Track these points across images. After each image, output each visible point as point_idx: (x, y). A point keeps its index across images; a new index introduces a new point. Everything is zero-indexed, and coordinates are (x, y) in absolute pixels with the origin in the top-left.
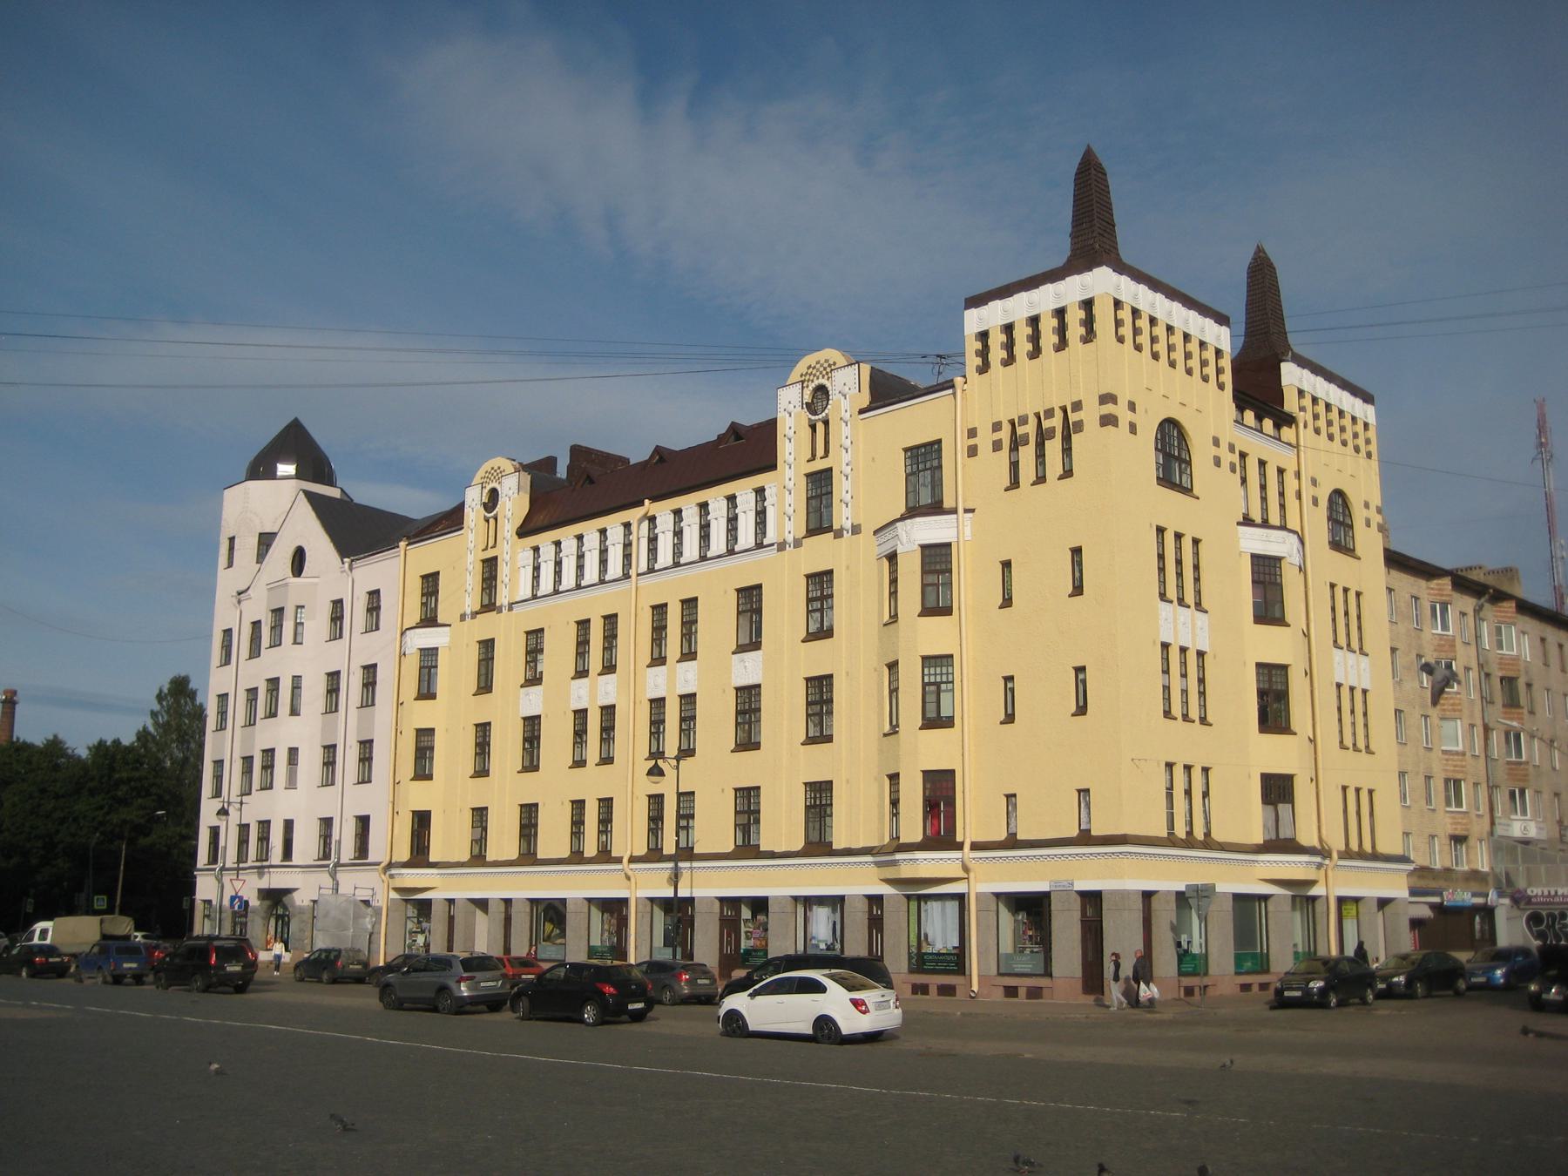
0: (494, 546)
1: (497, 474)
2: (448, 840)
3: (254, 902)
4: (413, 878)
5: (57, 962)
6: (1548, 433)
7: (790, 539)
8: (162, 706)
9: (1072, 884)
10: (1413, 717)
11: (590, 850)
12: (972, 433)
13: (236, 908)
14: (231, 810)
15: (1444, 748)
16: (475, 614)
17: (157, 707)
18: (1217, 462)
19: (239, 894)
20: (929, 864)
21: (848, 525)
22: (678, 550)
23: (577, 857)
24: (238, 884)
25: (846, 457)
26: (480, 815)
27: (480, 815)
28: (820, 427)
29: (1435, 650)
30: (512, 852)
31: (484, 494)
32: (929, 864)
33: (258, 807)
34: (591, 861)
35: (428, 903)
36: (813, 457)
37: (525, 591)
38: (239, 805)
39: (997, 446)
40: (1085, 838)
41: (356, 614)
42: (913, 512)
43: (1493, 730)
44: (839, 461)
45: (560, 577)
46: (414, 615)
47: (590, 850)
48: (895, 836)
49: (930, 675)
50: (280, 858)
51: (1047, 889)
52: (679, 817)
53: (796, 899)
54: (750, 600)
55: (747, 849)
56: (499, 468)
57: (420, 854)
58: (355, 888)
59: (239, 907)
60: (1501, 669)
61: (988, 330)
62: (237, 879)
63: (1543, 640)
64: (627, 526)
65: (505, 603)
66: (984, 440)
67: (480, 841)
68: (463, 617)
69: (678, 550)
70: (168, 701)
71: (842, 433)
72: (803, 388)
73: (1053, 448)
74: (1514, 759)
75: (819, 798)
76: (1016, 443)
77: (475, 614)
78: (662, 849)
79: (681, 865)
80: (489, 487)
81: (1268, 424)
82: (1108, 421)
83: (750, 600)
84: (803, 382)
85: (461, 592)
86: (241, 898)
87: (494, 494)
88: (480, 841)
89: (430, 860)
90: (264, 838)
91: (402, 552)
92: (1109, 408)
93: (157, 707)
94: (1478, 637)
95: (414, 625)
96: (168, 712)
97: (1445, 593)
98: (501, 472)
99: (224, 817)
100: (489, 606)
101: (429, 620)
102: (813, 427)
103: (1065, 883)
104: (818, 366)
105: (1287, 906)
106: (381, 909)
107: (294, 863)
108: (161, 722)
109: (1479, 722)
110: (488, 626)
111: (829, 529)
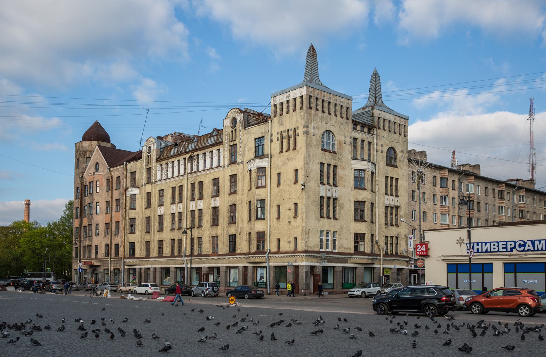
0: (235, 140)
2: (139, 251)
6: (534, 110)
7: (226, 165)
10: (152, 240)
14: (188, 231)
20: (259, 258)
22: (212, 165)
23: (173, 256)
28: (234, 132)
32: (259, 258)
35: (134, 269)
42: (257, 157)
43: (462, 217)
45: (206, 165)
52: (199, 245)
53: (227, 267)
54: (216, 182)
55: (215, 253)
57: (132, 255)
63: (486, 188)
69: (212, 165)
77: (145, 185)
79: (192, 258)
80: (149, 146)
83: (216, 182)
85: (142, 177)
97: (446, 174)
99: (185, 234)
105: (362, 270)
109: (457, 215)
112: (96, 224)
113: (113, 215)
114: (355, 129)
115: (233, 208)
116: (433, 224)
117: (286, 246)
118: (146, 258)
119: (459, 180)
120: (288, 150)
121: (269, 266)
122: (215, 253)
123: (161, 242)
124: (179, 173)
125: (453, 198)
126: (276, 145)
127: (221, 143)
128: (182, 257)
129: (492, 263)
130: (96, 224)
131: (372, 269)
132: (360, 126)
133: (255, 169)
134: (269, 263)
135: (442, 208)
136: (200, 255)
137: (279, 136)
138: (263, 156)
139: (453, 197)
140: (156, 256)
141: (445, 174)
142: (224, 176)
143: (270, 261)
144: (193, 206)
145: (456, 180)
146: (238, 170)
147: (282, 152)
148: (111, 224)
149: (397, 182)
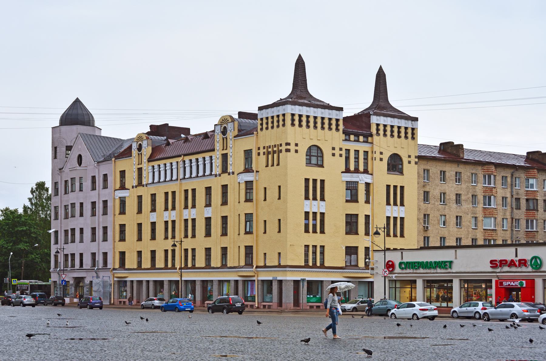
2: (131, 262)
3: (72, 282)
4: (121, 274)
8: (34, 196)
12: (259, 149)
13: (64, 284)
15: (484, 228)
17: (31, 196)
18: (334, 155)
19: (65, 279)
24: (64, 276)
25: (231, 151)
26: (140, 253)
27: (140, 253)
29: (484, 192)
33: (70, 248)
35: (126, 281)
36: (223, 150)
37: (150, 181)
39: (264, 153)
40: (279, 266)
41: (99, 182)
44: (229, 152)
46: (118, 186)
50: (79, 266)
51: (272, 279)
54: (208, 190)
58: (103, 277)
59: (65, 284)
60: (526, 196)
62: (64, 274)
64: (177, 162)
66: (262, 151)
67: (140, 263)
68: (133, 187)
70: (36, 193)
71: (230, 143)
72: (221, 126)
73: (275, 155)
76: (269, 153)
77: (136, 187)
80: (139, 143)
81: (361, 138)
82: (288, 150)
83: (208, 190)
84: (221, 124)
85: (131, 179)
86: (65, 281)
87: (140, 145)
88: (140, 263)
90: (73, 260)
91: (113, 162)
92: (288, 147)
93: (31, 196)
94: (427, 204)
96: (36, 198)
100: (140, 184)
101: (123, 187)
102: (223, 139)
106: (111, 284)
107: (84, 268)
108: (34, 203)
109: (509, 217)
110: (141, 191)
112: (80, 178)
115: (225, 219)
116: (471, 229)
119: (512, 175)
120: (273, 165)
121: (258, 280)
122: (208, 266)
125: (503, 198)
126: (263, 158)
127: (213, 150)
128: (176, 269)
129: (534, 279)
130: (80, 178)
131: (370, 283)
133: (244, 182)
134: (258, 276)
135: (485, 210)
136: (194, 267)
137: (265, 150)
139: (503, 196)
141: (489, 170)
142: (216, 185)
143: (259, 276)
145: (509, 176)
147: (267, 166)
149: (307, 226)
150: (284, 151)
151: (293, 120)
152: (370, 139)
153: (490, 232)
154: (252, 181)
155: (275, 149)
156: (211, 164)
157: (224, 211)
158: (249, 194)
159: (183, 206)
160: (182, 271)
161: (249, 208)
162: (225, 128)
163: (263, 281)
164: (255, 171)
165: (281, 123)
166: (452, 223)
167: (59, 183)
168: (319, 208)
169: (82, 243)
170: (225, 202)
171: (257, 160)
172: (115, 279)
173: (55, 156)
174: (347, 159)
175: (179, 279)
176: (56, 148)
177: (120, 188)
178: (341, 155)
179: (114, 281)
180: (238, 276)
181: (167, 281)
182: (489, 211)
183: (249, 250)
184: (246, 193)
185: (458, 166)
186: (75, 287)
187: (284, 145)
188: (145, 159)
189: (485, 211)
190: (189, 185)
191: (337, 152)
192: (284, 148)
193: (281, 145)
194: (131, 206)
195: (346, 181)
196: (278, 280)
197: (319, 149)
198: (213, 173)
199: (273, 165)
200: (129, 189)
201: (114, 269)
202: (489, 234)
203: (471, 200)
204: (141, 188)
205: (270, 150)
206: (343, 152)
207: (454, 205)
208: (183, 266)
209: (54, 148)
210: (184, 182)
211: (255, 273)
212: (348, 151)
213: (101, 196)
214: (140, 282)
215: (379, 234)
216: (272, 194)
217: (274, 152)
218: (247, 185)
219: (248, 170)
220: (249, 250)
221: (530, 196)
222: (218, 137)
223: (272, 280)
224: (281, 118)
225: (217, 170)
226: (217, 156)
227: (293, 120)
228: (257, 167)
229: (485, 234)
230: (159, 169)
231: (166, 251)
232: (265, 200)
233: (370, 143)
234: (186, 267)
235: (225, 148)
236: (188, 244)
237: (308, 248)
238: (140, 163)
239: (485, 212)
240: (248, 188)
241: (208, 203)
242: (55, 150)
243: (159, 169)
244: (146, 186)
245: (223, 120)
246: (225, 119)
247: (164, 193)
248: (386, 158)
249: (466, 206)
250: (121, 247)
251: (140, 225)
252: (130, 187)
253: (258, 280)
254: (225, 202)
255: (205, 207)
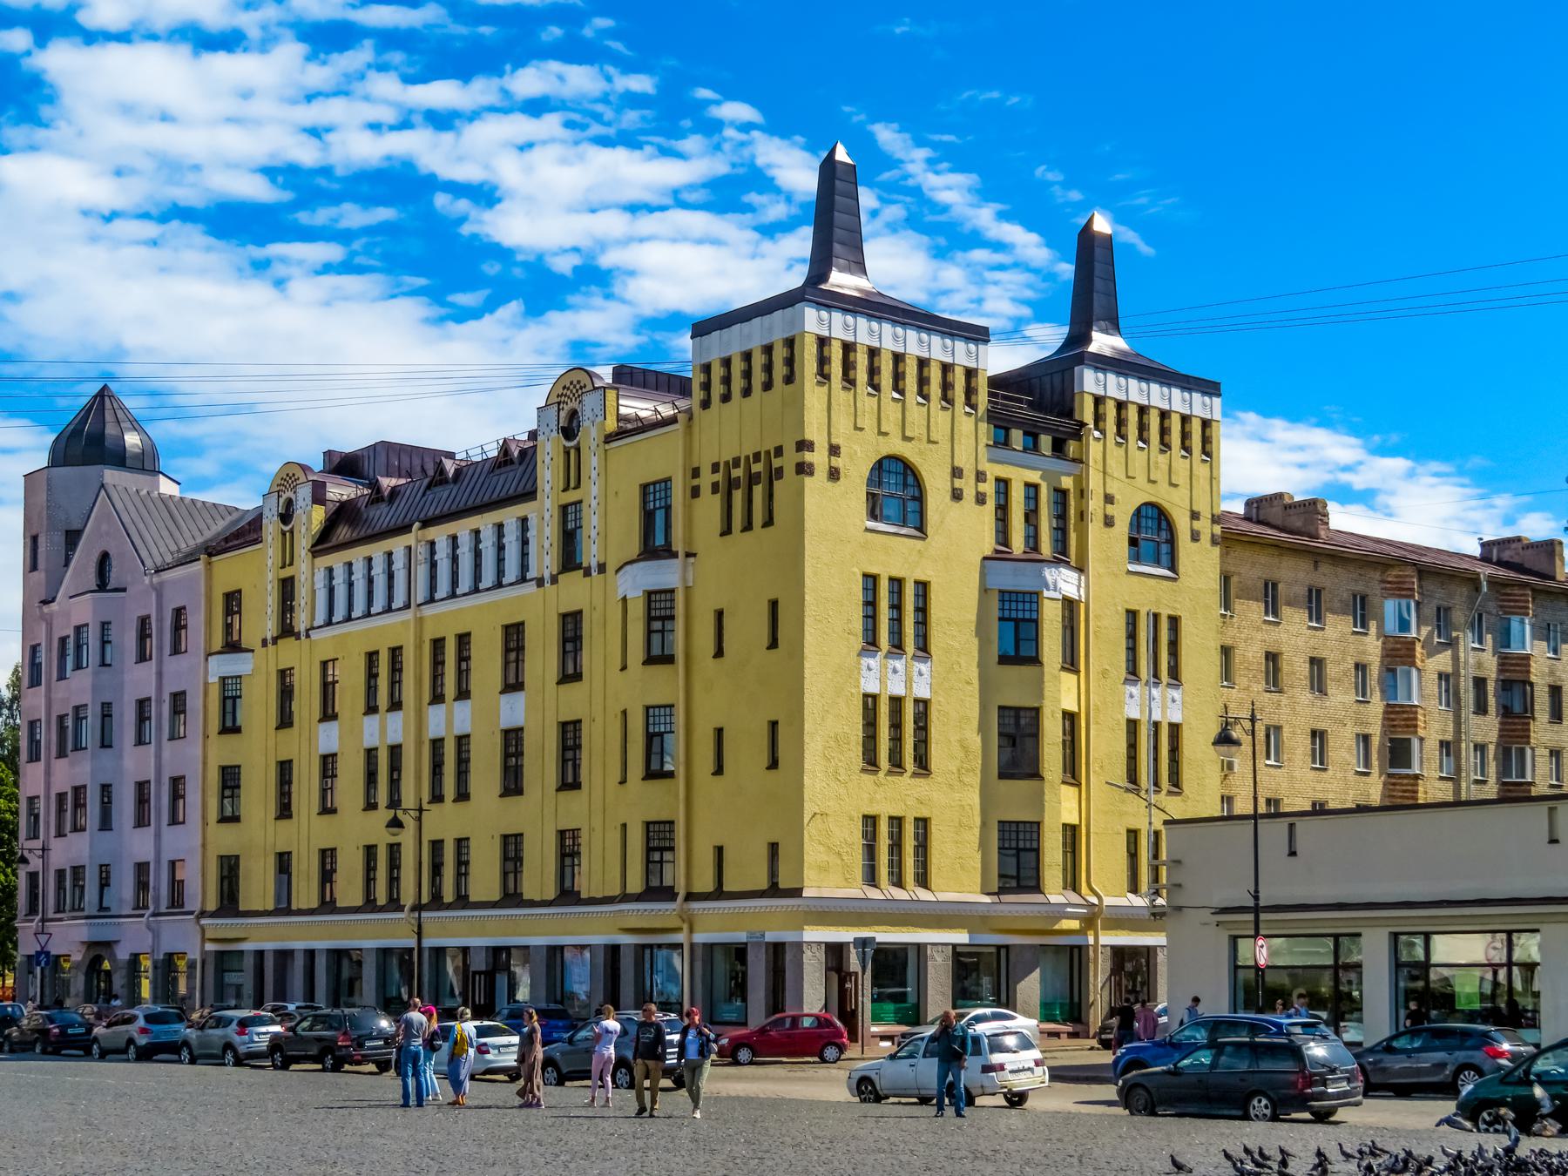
1: (577, 391)
2: (258, 888)
5: (1297, 1111)
7: (547, 576)
9: (763, 936)
11: (448, 895)
12: (696, 473)
16: (275, 640)
21: (594, 564)
23: (370, 905)
30: (358, 901)
31: (281, 504)
34: (449, 907)
36: (283, 567)
38: (417, 814)
39: (715, 488)
46: (218, 643)
47: (448, 895)
48: (328, 899)
49: (654, 724)
54: (514, 636)
56: (294, 475)
57: (229, 903)
61: (751, 350)
65: (302, 629)
66: (707, 479)
68: (264, 643)
73: (758, 491)
74: (1555, 783)
75: (568, 848)
76: (732, 484)
77: (275, 640)
78: (375, 900)
80: (285, 496)
83: (514, 636)
84: (559, 403)
85: (260, 619)
89: (241, 909)
95: (635, 557)
98: (581, 388)
100: (287, 630)
101: (233, 647)
102: (567, 453)
103: (758, 935)
104: (571, 387)
110: (289, 653)
111: (579, 567)
113: (163, 762)
114: (1003, 443)
115: (570, 735)
117: (748, 871)
118: (277, 912)
120: (748, 527)
121: (692, 946)
123: (328, 858)
124: (390, 598)
126: (710, 506)
127: (530, 495)
128: (400, 909)
132: (1020, 432)
134: (691, 931)
135: (1392, 713)
136: (462, 901)
137: (719, 477)
138: (668, 552)
140: (1494, 797)
141: (1404, 583)
143: (696, 927)
144: (438, 721)
146: (636, 582)
148: (419, 698)
150: (789, 471)
151: (823, 361)
152: (1072, 447)
153: (1407, 785)
154: (672, 591)
155: (757, 468)
156: (525, 542)
157: (572, 702)
158: (660, 628)
159: (427, 697)
160: (424, 914)
161: (662, 686)
162: (574, 414)
163: (710, 947)
164: (681, 554)
165: (779, 370)
166: (1299, 751)
167: (43, 644)
168: (909, 682)
169: (107, 833)
170: (571, 675)
171: (688, 511)
172: (210, 947)
173: (32, 564)
174: (1003, 510)
175: (411, 942)
176: (35, 539)
177: (225, 650)
178: (981, 499)
179: (204, 953)
180: (620, 929)
181: (823, 946)
182: (1405, 716)
183: (659, 838)
184: (650, 632)
185: (1316, 567)
186: (87, 974)
187: (789, 449)
188: (303, 543)
189: (1392, 716)
190: (446, 618)
191: (968, 485)
192: (788, 461)
193: (779, 451)
194: (258, 707)
195: (1000, 591)
196: (767, 943)
197: (909, 472)
198: (529, 576)
199: (748, 527)
200: (253, 651)
201: (203, 914)
202: (1405, 791)
203: (1353, 680)
204: (289, 642)
205: (737, 473)
206: (988, 488)
207: (1305, 697)
208: (425, 900)
209: (28, 540)
210: (429, 611)
211: (683, 921)
212: (1003, 485)
213: (165, 681)
214: (284, 956)
215: (1237, 743)
216: (747, 629)
217: (753, 479)
218: (653, 605)
219: (654, 548)
220: (659, 838)
221: (1515, 671)
222: (549, 447)
223: (746, 944)
224: (779, 354)
225: (545, 559)
226: (543, 515)
227: (823, 361)
228: (689, 540)
229: (1394, 790)
230: (350, 578)
231: (370, 851)
232: (719, 653)
233: (1074, 460)
234: (437, 902)
235: (572, 484)
236: (445, 822)
237: (874, 825)
238: (288, 560)
239: (1393, 720)
240: (658, 613)
241: (512, 680)
242: (33, 543)
243: (350, 578)
244: (308, 636)
245: (564, 388)
246: (571, 383)
247: (363, 656)
248: (1123, 514)
249: (1340, 698)
250: (225, 840)
251: (285, 768)
252: (257, 645)
253: (692, 946)
254: (571, 675)
255: (501, 693)
